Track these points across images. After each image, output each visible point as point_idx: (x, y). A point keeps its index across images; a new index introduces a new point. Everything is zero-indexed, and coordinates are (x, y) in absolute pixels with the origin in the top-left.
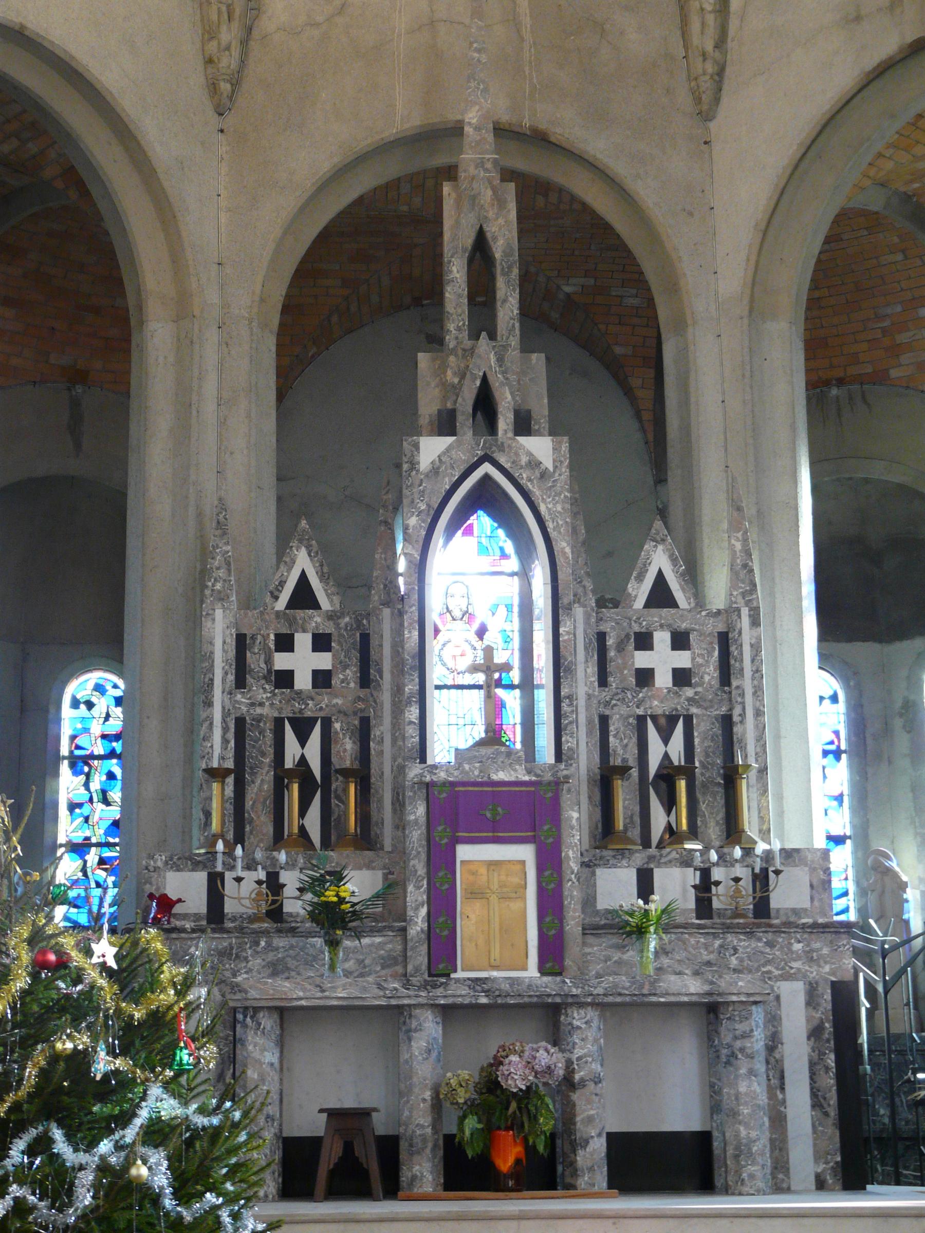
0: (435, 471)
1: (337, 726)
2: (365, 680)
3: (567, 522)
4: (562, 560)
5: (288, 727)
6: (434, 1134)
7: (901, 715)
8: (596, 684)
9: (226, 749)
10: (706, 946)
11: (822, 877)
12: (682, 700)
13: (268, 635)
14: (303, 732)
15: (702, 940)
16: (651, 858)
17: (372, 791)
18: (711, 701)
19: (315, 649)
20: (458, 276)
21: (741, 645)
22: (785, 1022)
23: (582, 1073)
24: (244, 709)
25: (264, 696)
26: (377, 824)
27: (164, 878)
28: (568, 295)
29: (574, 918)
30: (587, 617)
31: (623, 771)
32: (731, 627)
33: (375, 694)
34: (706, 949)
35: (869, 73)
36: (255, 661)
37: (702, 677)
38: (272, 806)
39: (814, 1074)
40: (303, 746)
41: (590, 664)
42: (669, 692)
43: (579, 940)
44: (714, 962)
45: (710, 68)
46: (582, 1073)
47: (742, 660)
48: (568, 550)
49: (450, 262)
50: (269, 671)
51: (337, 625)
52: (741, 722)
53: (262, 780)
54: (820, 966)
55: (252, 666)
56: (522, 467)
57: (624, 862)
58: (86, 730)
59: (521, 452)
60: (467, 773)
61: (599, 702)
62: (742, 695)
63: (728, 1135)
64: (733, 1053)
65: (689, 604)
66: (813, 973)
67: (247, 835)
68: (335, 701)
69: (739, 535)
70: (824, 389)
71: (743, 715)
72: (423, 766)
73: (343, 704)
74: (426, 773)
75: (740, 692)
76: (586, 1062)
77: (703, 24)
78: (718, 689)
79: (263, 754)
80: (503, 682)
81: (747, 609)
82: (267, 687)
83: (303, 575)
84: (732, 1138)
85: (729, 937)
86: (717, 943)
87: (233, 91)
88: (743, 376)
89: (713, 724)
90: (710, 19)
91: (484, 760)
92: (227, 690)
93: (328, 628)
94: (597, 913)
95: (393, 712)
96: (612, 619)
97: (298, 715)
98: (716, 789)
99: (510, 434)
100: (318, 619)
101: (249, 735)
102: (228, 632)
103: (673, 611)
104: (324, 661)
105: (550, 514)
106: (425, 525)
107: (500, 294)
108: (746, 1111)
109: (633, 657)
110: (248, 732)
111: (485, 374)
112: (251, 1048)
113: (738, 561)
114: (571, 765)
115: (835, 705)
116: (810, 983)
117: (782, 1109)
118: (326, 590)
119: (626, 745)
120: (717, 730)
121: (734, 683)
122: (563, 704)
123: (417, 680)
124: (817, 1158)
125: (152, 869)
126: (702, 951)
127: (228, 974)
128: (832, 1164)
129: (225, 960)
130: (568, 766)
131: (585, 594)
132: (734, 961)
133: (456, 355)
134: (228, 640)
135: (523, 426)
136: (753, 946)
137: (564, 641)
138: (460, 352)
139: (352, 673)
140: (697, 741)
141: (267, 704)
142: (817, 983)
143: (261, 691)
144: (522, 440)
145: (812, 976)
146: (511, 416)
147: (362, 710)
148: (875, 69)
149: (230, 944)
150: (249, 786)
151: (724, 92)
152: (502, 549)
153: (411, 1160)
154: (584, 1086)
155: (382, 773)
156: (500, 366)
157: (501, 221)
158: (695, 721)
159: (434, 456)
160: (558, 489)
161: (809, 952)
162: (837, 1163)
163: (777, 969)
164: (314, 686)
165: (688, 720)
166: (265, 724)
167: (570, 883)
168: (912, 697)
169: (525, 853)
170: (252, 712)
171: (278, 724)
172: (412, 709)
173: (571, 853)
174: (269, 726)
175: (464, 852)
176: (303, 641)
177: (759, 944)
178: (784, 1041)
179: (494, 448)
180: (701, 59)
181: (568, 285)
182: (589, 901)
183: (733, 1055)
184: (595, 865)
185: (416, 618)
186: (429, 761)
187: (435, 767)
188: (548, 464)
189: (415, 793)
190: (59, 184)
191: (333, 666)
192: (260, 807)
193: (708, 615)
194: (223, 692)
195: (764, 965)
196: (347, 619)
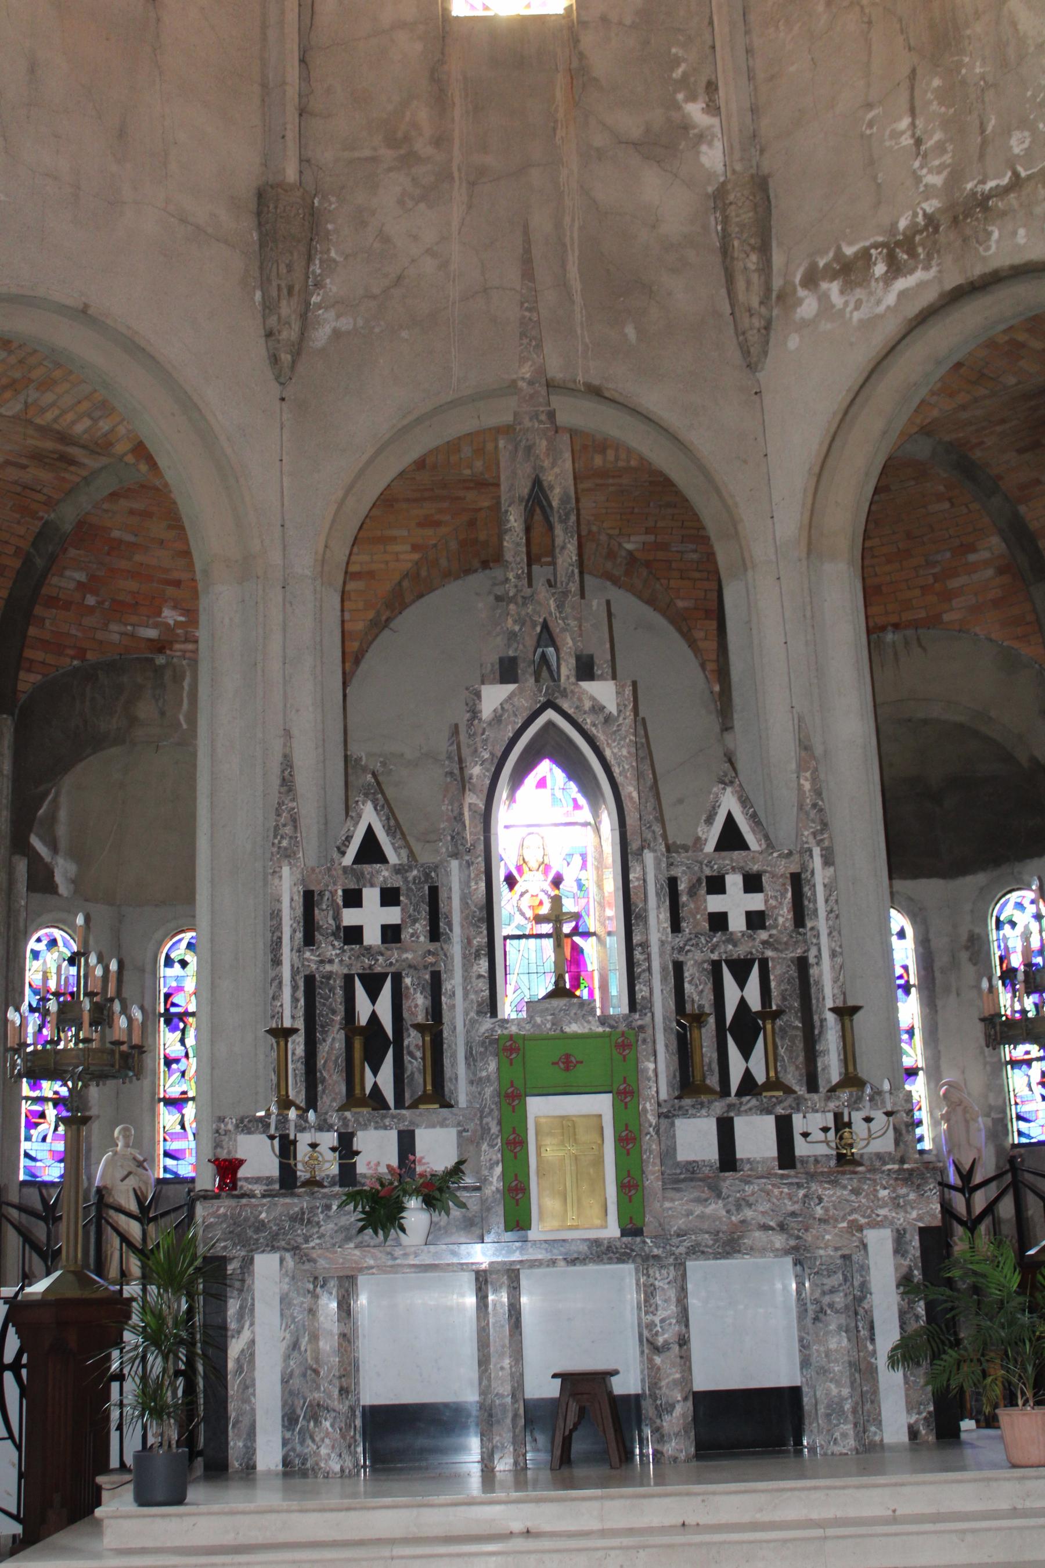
0: (497, 719)
1: (408, 981)
2: (435, 934)
3: (632, 766)
4: (629, 805)
5: (358, 984)
6: (513, 1403)
7: (967, 948)
8: (669, 930)
9: (296, 1008)
10: (790, 1197)
11: (905, 1119)
12: (757, 943)
13: (336, 891)
14: (373, 986)
15: (786, 1190)
16: (730, 1107)
17: (445, 1046)
18: (786, 943)
19: (384, 903)
20: (516, 524)
21: (814, 886)
22: (872, 1271)
23: (666, 1336)
24: (314, 966)
25: (334, 953)
26: (451, 1079)
27: (235, 1140)
28: (630, 553)
29: (653, 1173)
30: (658, 862)
31: (698, 1019)
32: (804, 867)
33: (445, 947)
34: (791, 1199)
35: (911, 320)
36: (323, 918)
37: (776, 919)
38: (344, 1064)
39: (905, 1323)
40: (373, 1002)
41: (662, 909)
42: (743, 935)
43: (660, 1194)
44: (798, 1212)
45: (757, 322)
46: (666, 1336)
47: (815, 902)
48: (635, 795)
49: (507, 511)
50: (338, 927)
51: (406, 880)
52: (817, 964)
53: (334, 1039)
54: (906, 1212)
55: (321, 923)
56: (585, 713)
57: (704, 1112)
58: (180, 989)
59: (584, 697)
60: (539, 1026)
61: (673, 948)
62: (818, 936)
63: (818, 1394)
64: (822, 1308)
65: (760, 845)
66: (900, 1219)
67: (319, 1094)
68: (405, 956)
69: (808, 774)
70: (881, 635)
71: (819, 957)
72: (494, 1020)
73: (413, 958)
74: (497, 1028)
75: (815, 933)
76: (670, 1324)
77: (748, 283)
78: (793, 931)
79: (334, 1012)
80: (580, 930)
81: (818, 849)
82: (336, 943)
83: (370, 830)
84: (823, 1397)
85: (814, 1186)
86: (801, 1193)
87: (294, 362)
88: (804, 616)
89: (789, 966)
90: (755, 278)
91: (556, 1012)
92: (296, 947)
93: (396, 882)
94: (678, 1164)
95: (464, 965)
96: (682, 864)
97: (368, 971)
98: (794, 1033)
99: (573, 679)
100: (386, 873)
101: (319, 993)
102: (295, 889)
103: (744, 853)
104: (393, 915)
105: (616, 759)
106: (489, 774)
107: (559, 542)
108: (836, 1369)
109: (705, 901)
110: (319, 990)
111: (545, 620)
112: (322, 1319)
113: (808, 801)
114: (646, 1014)
115: (903, 941)
116: (898, 1231)
117: (873, 1360)
118: (393, 844)
119: (702, 991)
120: (793, 972)
121: (809, 924)
122: (636, 952)
123: (485, 932)
124: (909, 1411)
125: (223, 1133)
126: (786, 1201)
127: (300, 1240)
128: (924, 1414)
129: (297, 1225)
130: (643, 1015)
131: (655, 839)
132: (819, 1211)
133: (516, 603)
134: (296, 898)
135: (586, 670)
136: (838, 1194)
137: (635, 887)
138: (520, 600)
139: (421, 927)
140: (773, 984)
141: (337, 960)
142: (904, 1230)
143: (330, 948)
144: (585, 685)
145: (899, 1222)
146: (573, 661)
147: (432, 964)
148: (917, 316)
149: (302, 1209)
150: (321, 1044)
151: (771, 344)
152: (575, 800)
153: (491, 1431)
154: (669, 1349)
155: (455, 1028)
156: (560, 613)
157: (557, 470)
158: (770, 964)
159: (496, 704)
160: (623, 732)
161: (895, 1198)
162: (929, 1413)
163: (863, 1216)
164: (384, 941)
165: (764, 964)
166: (335, 981)
167: (648, 1137)
168: (977, 930)
169: (602, 1104)
170: (321, 969)
171: (349, 980)
172: (481, 962)
173: (648, 1105)
174: (339, 982)
175: (538, 1107)
176: (371, 896)
177: (845, 1193)
178: (873, 1290)
179: (557, 694)
180: (748, 314)
181: (629, 542)
182: (668, 1153)
183: (822, 1310)
184: (674, 1116)
185: (483, 869)
186: (500, 1016)
187: (506, 1021)
188: (612, 708)
189: (486, 1049)
190: (130, 459)
191: (402, 920)
192: (331, 1064)
193: (779, 856)
194: (292, 950)
195: (851, 1213)
196: (415, 872)
